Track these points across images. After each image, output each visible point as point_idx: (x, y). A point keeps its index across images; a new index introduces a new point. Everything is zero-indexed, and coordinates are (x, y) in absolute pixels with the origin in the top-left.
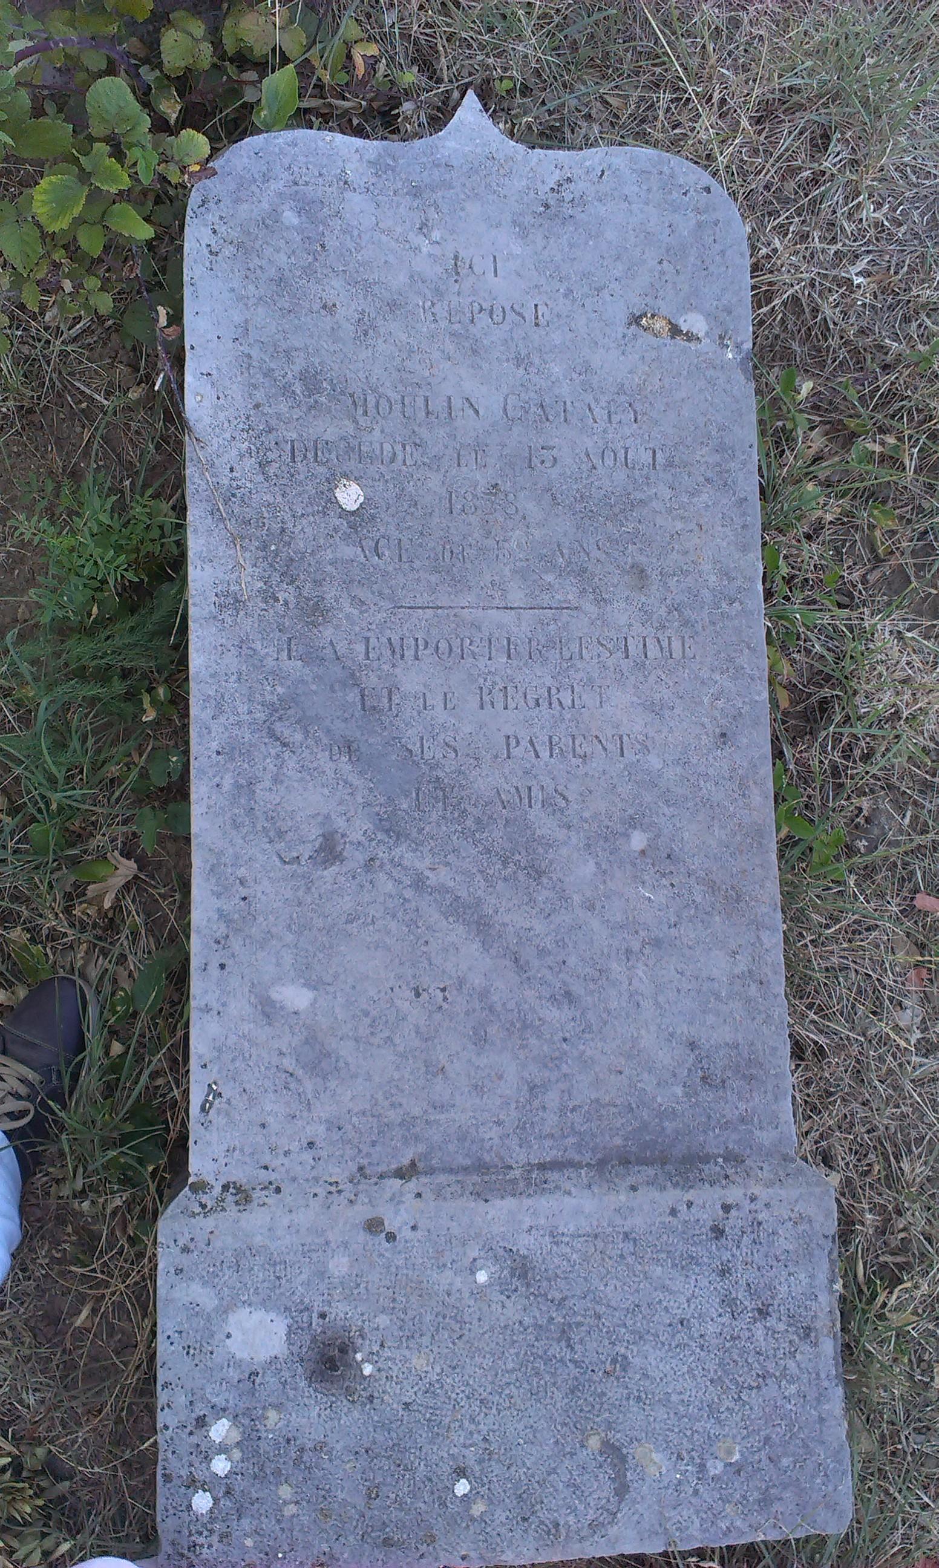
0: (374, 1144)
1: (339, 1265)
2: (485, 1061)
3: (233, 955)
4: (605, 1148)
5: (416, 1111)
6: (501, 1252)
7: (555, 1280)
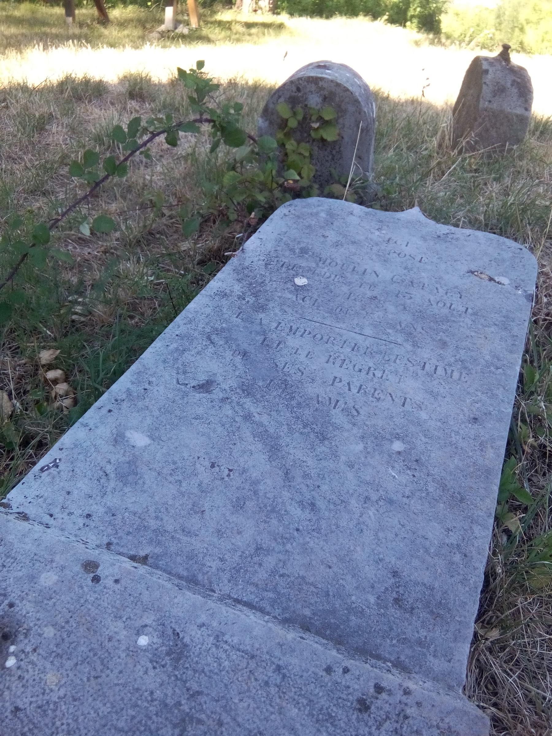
0: (129, 533)
1: (48, 579)
2: (235, 519)
3: (120, 409)
4: (294, 612)
5: (170, 528)
6: (170, 632)
7: (200, 674)
